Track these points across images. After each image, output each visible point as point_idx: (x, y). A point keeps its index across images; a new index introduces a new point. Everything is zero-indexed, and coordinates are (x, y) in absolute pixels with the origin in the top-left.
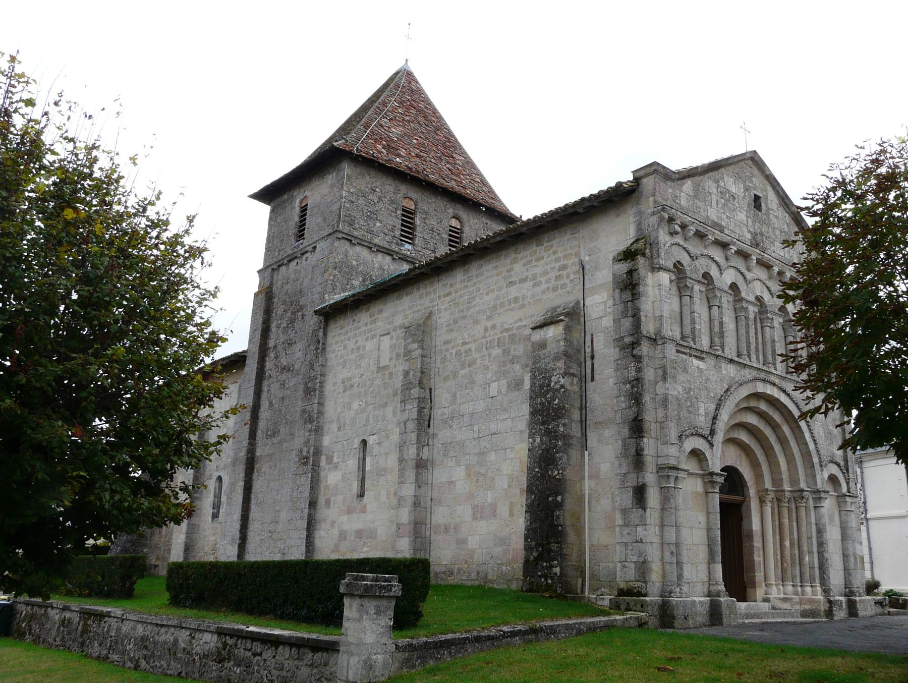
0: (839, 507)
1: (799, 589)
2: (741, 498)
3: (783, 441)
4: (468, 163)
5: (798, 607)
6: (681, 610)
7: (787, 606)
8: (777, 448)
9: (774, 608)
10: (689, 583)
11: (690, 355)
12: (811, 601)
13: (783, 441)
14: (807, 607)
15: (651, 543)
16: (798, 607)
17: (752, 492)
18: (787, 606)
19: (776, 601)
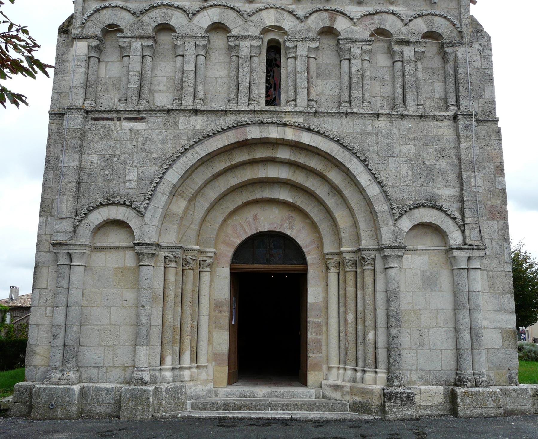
0: (451, 264)
1: (359, 374)
2: (300, 266)
3: (335, 190)
4: (473, 21)
5: (348, 398)
6: (44, 398)
7: (337, 395)
8: (331, 202)
9: (324, 397)
10: (98, 367)
11: (119, 119)
12: (364, 392)
13: (335, 190)
14: (358, 399)
15: (37, 325)
16: (348, 398)
17: (311, 258)
18: (337, 395)
19: (327, 388)
